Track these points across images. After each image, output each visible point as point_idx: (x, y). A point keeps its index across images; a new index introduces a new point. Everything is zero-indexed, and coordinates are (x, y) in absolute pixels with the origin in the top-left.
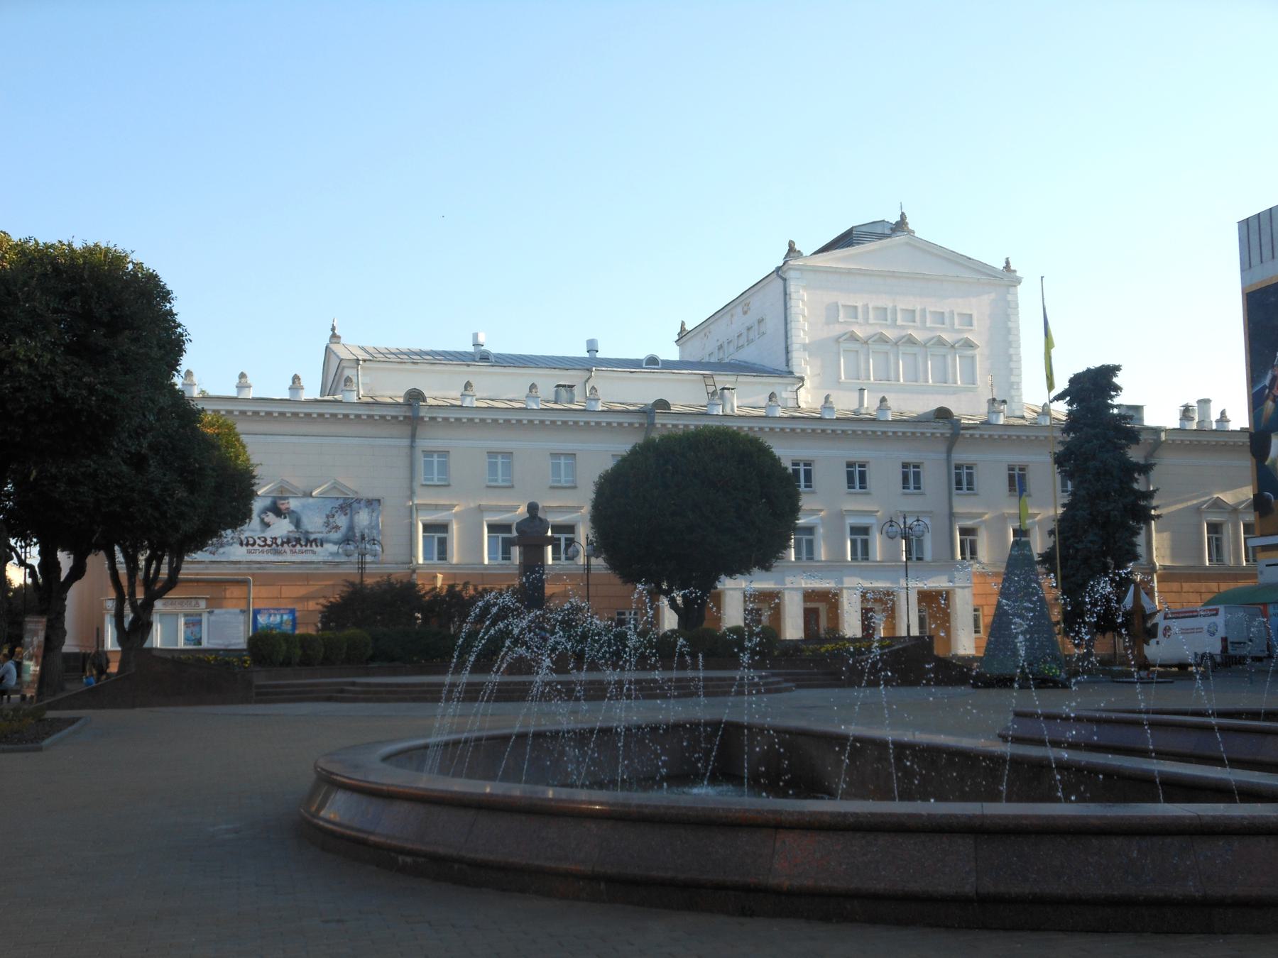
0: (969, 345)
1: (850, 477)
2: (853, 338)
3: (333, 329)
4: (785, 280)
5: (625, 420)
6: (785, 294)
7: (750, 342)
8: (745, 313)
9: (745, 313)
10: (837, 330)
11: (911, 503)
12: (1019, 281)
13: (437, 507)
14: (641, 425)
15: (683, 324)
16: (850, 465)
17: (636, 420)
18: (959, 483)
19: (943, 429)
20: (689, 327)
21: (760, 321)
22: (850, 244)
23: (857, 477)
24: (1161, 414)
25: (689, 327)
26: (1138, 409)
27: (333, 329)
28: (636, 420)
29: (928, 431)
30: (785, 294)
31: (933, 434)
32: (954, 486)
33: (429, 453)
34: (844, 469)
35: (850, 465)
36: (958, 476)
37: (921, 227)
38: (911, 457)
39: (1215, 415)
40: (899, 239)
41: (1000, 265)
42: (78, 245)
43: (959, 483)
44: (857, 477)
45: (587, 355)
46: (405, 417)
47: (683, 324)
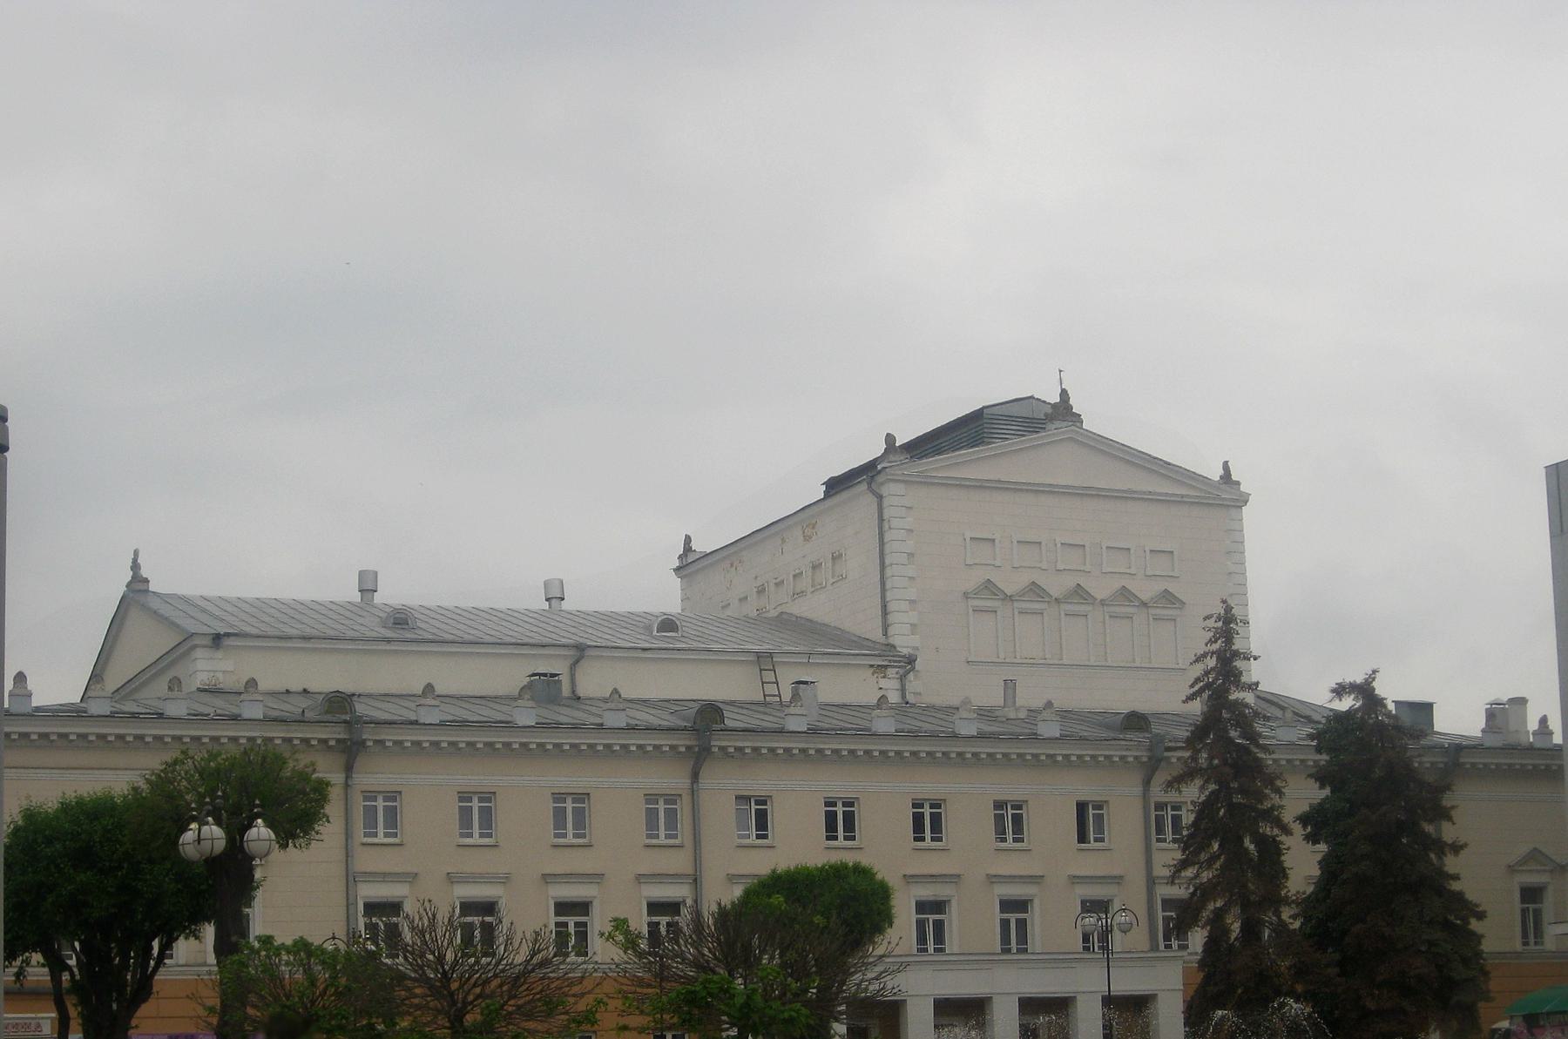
0: (1168, 598)
1: (831, 819)
2: (989, 587)
3: (135, 566)
4: (880, 498)
5: (665, 741)
6: (881, 519)
7: (817, 588)
8: (807, 538)
9: (807, 538)
10: (973, 580)
11: (1090, 863)
12: (1243, 500)
13: (385, 877)
14: (689, 748)
15: (688, 539)
16: (999, 805)
17: (682, 742)
18: (370, 821)
19: (1134, 747)
20: (700, 546)
21: (836, 558)
22: (977, 440)
23: (1010, 821)
24: (1459, 718)
25: (700, 546)
26: (1426, 708)
27: (135, 566)
28: (682, 742)
29: (1116, 754)
30: (881, 519)
31: (1122, 758)
32: (1154, 836)
33: (370, 796)
34: (991, 813)
35: (999, 805)
36: (371, 813)
37: (1096, 417)
38: (1088, 793)
39: (1533, 725)
40: (1057, 429)
41: (1215, 474)
42: (879, 877)
43: (370, 821)
44: (1010, 821)
45: (546, 606)
46: (338, 741)
47: (688, 539)
